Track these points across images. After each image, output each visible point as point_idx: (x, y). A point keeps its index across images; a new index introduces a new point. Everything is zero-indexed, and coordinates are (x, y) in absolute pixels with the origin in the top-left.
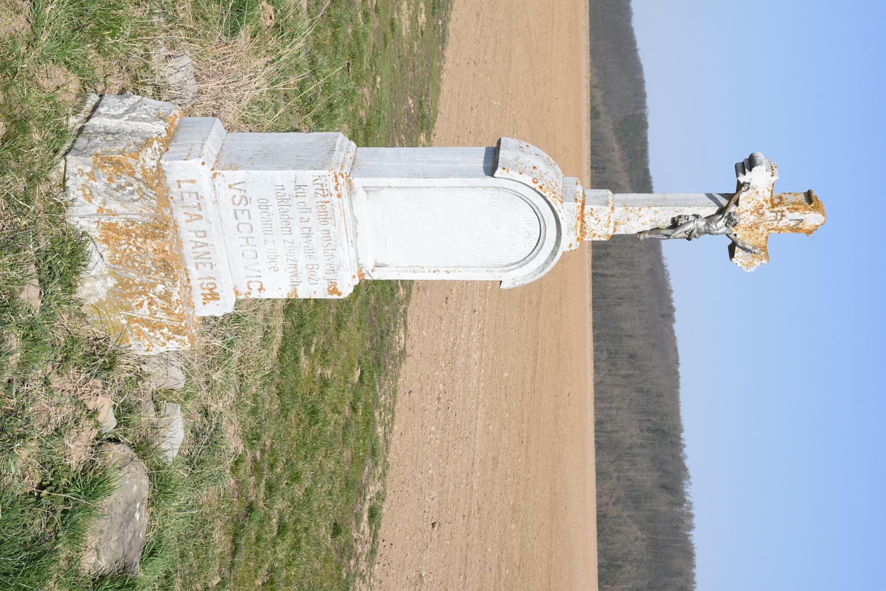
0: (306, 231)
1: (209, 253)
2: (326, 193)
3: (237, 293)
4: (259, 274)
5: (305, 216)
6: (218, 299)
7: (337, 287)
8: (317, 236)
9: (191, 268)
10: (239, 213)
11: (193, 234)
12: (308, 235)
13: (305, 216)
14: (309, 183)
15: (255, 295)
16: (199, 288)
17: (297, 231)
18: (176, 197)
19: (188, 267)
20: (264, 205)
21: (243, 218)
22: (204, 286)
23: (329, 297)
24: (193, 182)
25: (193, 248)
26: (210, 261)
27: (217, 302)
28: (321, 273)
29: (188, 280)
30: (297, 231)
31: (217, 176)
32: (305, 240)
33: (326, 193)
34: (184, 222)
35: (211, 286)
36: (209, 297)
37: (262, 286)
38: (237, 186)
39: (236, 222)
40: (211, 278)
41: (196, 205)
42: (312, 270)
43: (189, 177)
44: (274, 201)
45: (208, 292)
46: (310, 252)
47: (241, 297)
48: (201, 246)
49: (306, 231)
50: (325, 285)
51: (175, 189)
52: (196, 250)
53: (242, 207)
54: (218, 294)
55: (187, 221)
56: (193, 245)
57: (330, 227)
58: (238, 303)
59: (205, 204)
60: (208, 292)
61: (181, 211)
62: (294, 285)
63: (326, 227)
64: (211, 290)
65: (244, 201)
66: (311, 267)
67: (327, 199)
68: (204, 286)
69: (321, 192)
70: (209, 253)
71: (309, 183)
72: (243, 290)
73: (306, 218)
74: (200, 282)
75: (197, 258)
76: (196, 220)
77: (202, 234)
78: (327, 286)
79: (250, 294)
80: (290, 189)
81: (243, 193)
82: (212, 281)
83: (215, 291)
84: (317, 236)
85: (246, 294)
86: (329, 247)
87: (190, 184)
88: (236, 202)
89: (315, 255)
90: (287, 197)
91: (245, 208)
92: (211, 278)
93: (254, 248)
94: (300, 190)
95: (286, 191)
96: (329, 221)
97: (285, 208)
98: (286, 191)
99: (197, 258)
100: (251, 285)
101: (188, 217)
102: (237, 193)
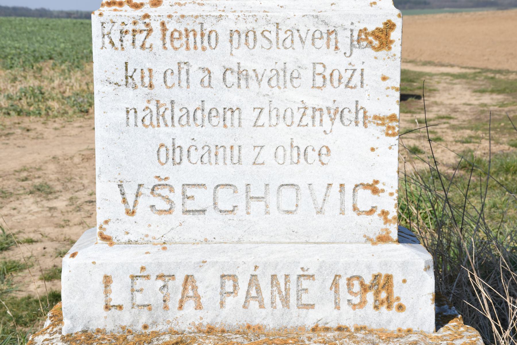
0: (231, 78)
1: (274, 277)
2: (141, 26)
3: (383, 239)
4: (336, 188)
5: (196, 76)
6: (389, 278)
7: (371, 28)
8: (243, 57)
9: (311, 318)
10: (190, 205)
11: (229, 300)
12: (242, 75)
13: (196, 76)
14: (120, 57)
15: (389, 203)
16: (359, 312)
17: (232, 97)
18: (144, 318)
19: (310, 323)
20: (173, 153)
21: (202, 198)
22: (356, 300)
23: (396, 48)
24: (107, 280)
25: (262, 306)
26: (293, 278)
27: (397, 281)
28: (335, 61)
29: (340, 329)
30: (232, 97)
31: (106, 233)
32: (253, 83)
33: (141, 26)
34: (199, 313)
35: (357, 287)
36: (383, 295)
37: (366, 186)
38: (131, 199)
39: (211, 212)
40: (335, 284)
41: (160, 283)
42: (327, 78)
43: (98, 284)
44: (164, 134)
45: (370, 296)
46: (285, 76)
47: (394, 231)
48: (258, 290)
49: (231, 78)
50: (365, 57)
51: (126, 318)
52: (267, 301)
53: (177, 197)
54: (376, 277)
55: (199, 307)
56: (254, 305)
57: (222, 29)
58: (406, 236)
59: (160, 265)
60: (370, 296)
61: (173, 312)
62: (364, 118)
63: (224, 38)
64: (365, 289)
65: (165, 192)
66: (319, 80)
67: (156, 26)
68: (356, 300)
69: (139, 38)
70: (274, 277)
71: (120, 57)
72: (375, 225)
73: (201, 75)
74: (344, 305)
75: (286, 301)
76: (195, 288)
77: (229, 286)
78: (369, 51)
79: (384, 213)
80: (134, 98)
81: (146, 191)
82: (343, 282)
83: (368, 280)
84: (243, 57)
85: (386, 221)
86: (272, 36)
87: (114, 286)
88: (164, 205)
89: (290, 67)
90: (153, 106)
91: (178, 190)
92: (335, 284)
93: (273, 188)
94: (137, 77)
95: (140, 107)
96: (208, 27)
97: (177, 114)
98: (140, 107)
99: (286, 301)
100: (364, 207)
101: (190, 305)
102: (144, 202)
